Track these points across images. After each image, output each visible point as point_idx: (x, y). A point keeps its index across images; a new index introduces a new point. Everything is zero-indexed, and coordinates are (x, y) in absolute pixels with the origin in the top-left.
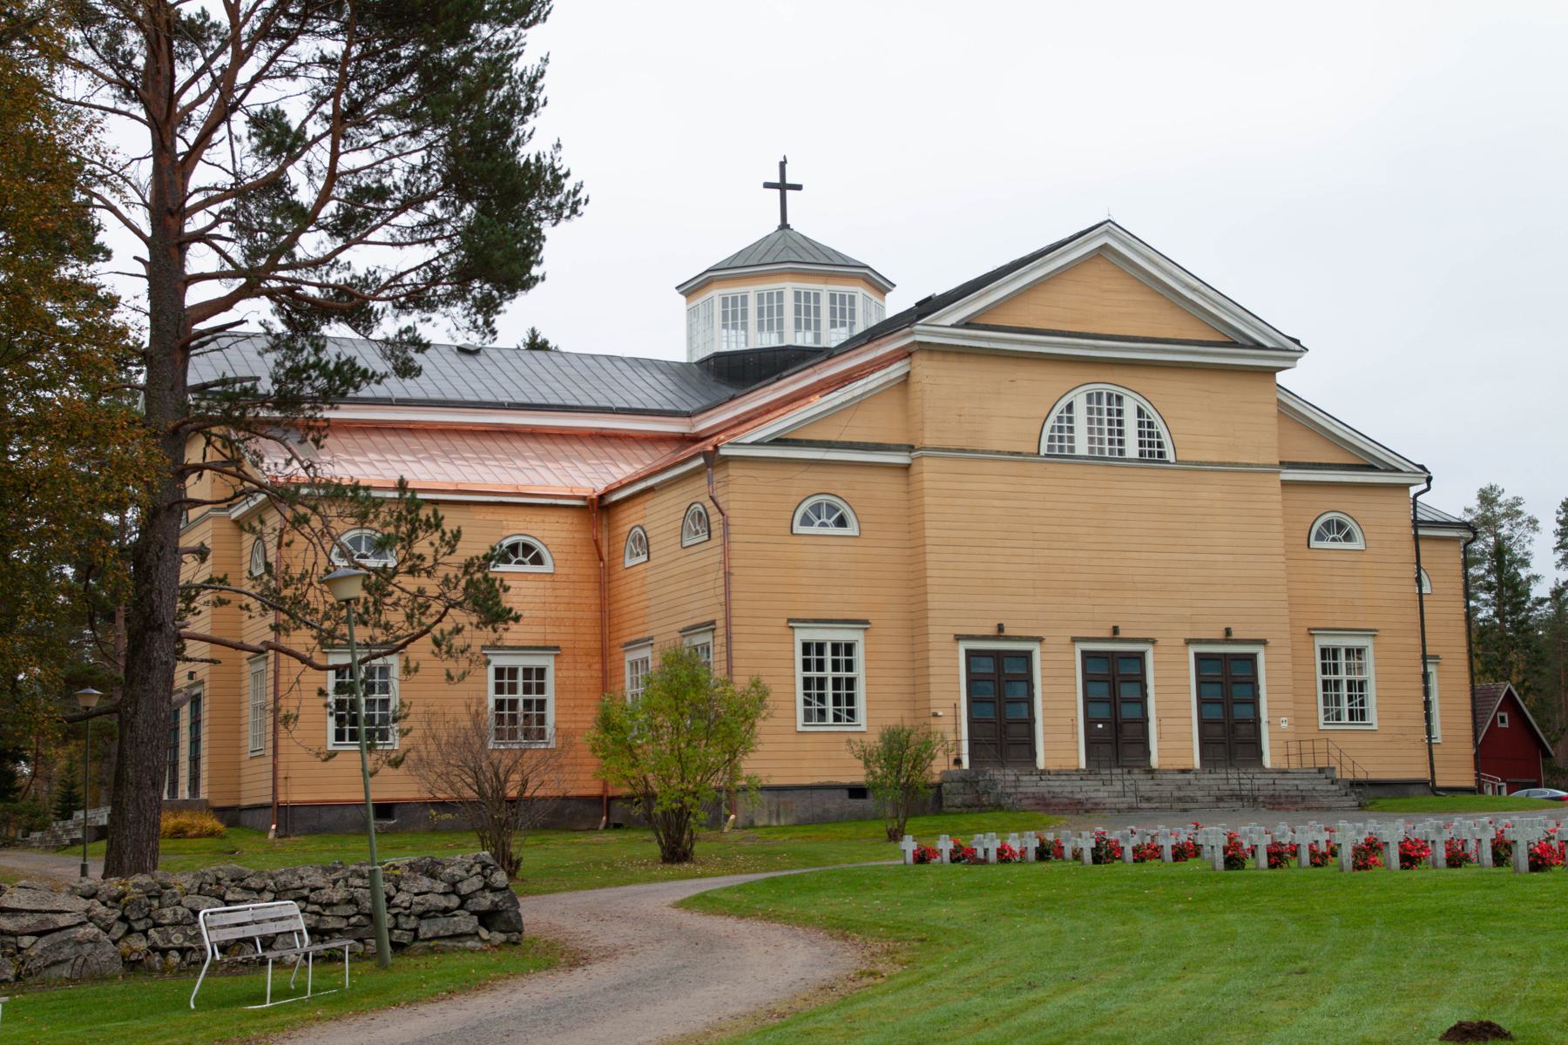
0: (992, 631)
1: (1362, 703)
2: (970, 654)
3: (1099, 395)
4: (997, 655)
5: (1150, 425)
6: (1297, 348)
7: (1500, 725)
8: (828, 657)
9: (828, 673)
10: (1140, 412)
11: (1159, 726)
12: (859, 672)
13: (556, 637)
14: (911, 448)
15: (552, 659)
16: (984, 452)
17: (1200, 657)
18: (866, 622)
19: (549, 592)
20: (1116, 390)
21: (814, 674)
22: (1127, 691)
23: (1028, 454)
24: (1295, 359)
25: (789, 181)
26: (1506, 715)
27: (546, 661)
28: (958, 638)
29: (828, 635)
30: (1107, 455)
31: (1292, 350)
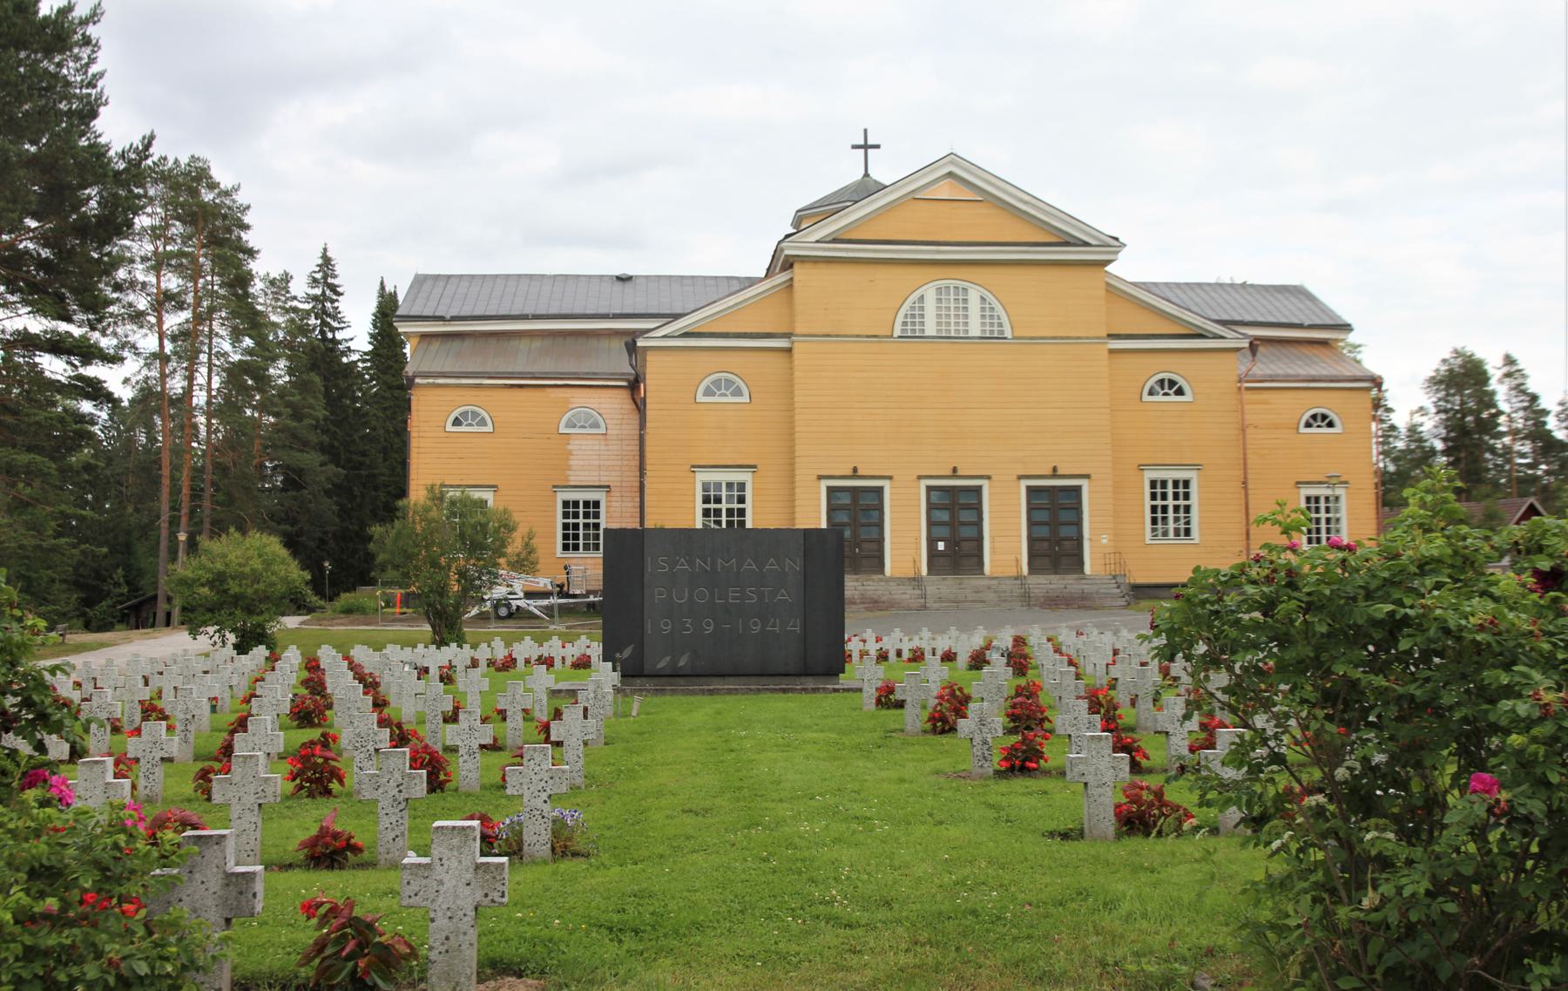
0: (849, 472)
2: (830, 490)
5: (992, 309)
8: (1170, 490)
9: (1170, 502)
10: (983, 299)
12: (1194, 501)
13: (606, 479)
14: (787, 335)
16: (837, 336)
17: (1030, 490)
18: (755, 467)
19: (603, 448)
20: (962, 284)
21: (1159, 502)
22: (965, 516)
23: (887, 337)
24: (1117, 252)
25: (869, 143)
28: (820, 478)
29: (1170, 475)
30: (953, 334)
31: (1114, 245)
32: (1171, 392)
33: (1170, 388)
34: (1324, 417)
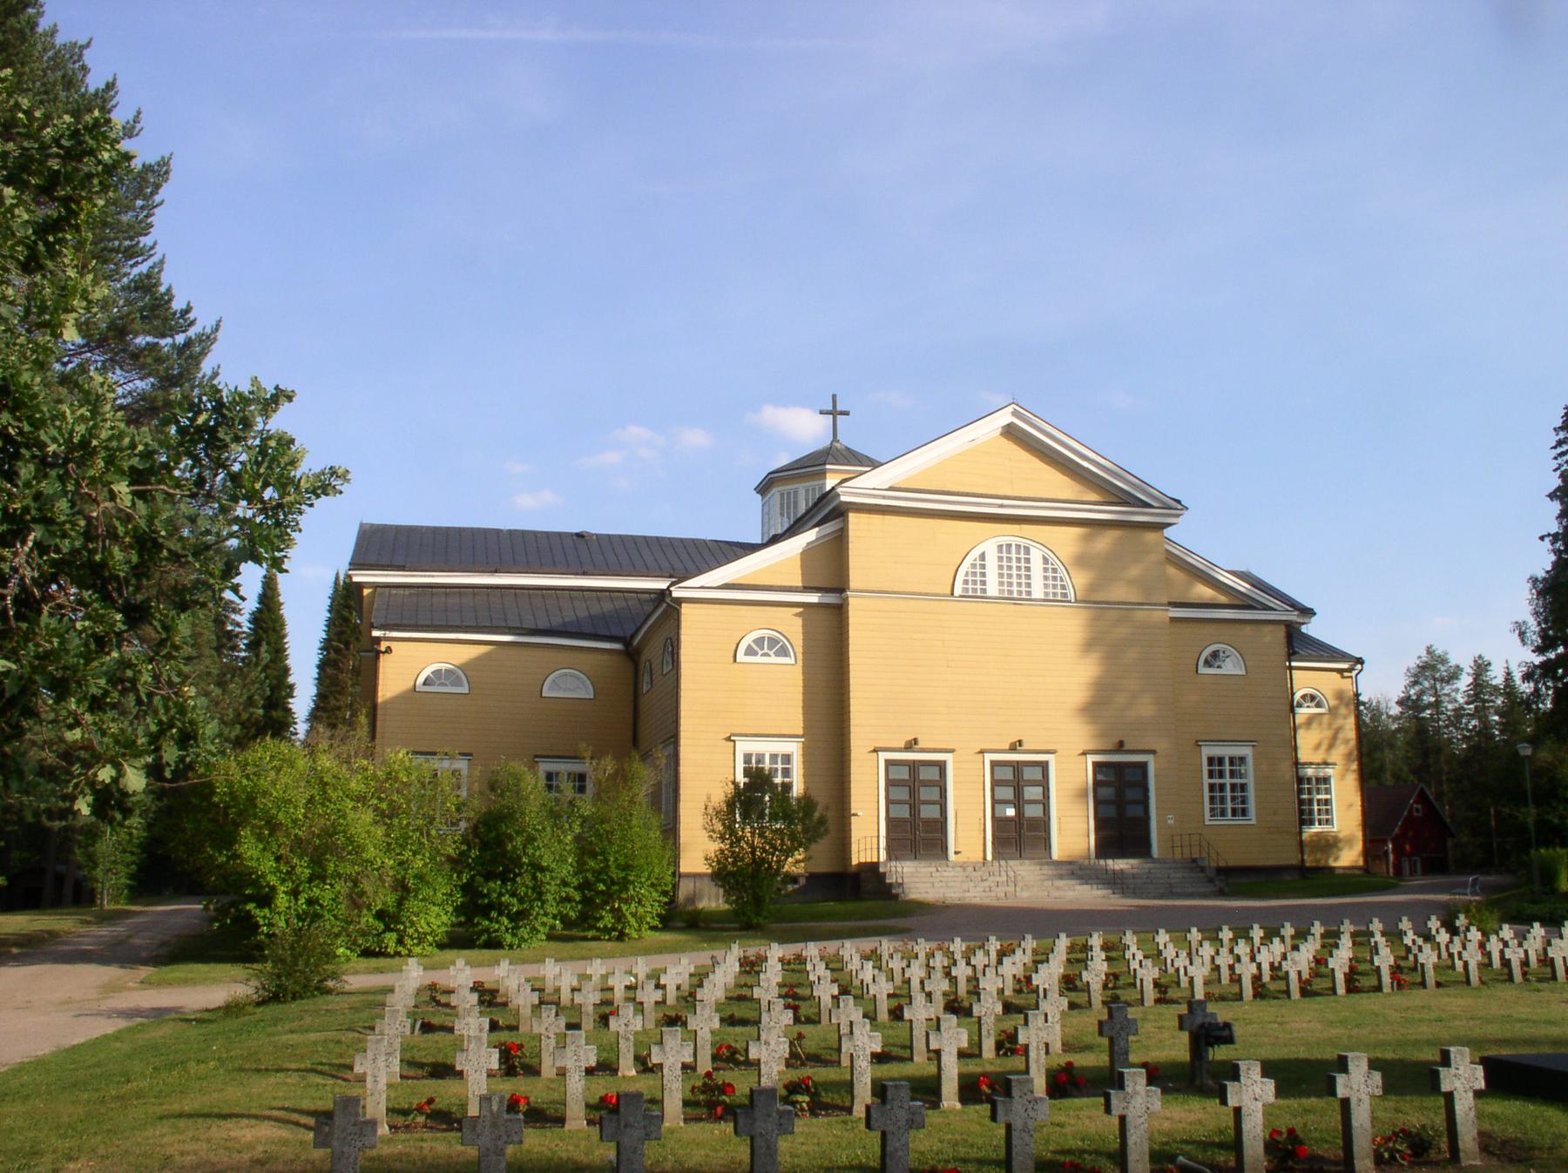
1: (1243, 802)
3: (1009, 546)
4: (914, 766)
6: (1180, 507)
7: (1415, 814)
10: (1046, 560)
11: (1059, 823)
15: (466, 762)
20: (1022, 542)
21: (1217, 781)
22: (1131, 794)
23: (944, 595)
26: (1419, 806)
27: (1246, 751)
31: (1175, 506)
32: (771, 653)
33: (770, 648)
34: (1313, 698)
